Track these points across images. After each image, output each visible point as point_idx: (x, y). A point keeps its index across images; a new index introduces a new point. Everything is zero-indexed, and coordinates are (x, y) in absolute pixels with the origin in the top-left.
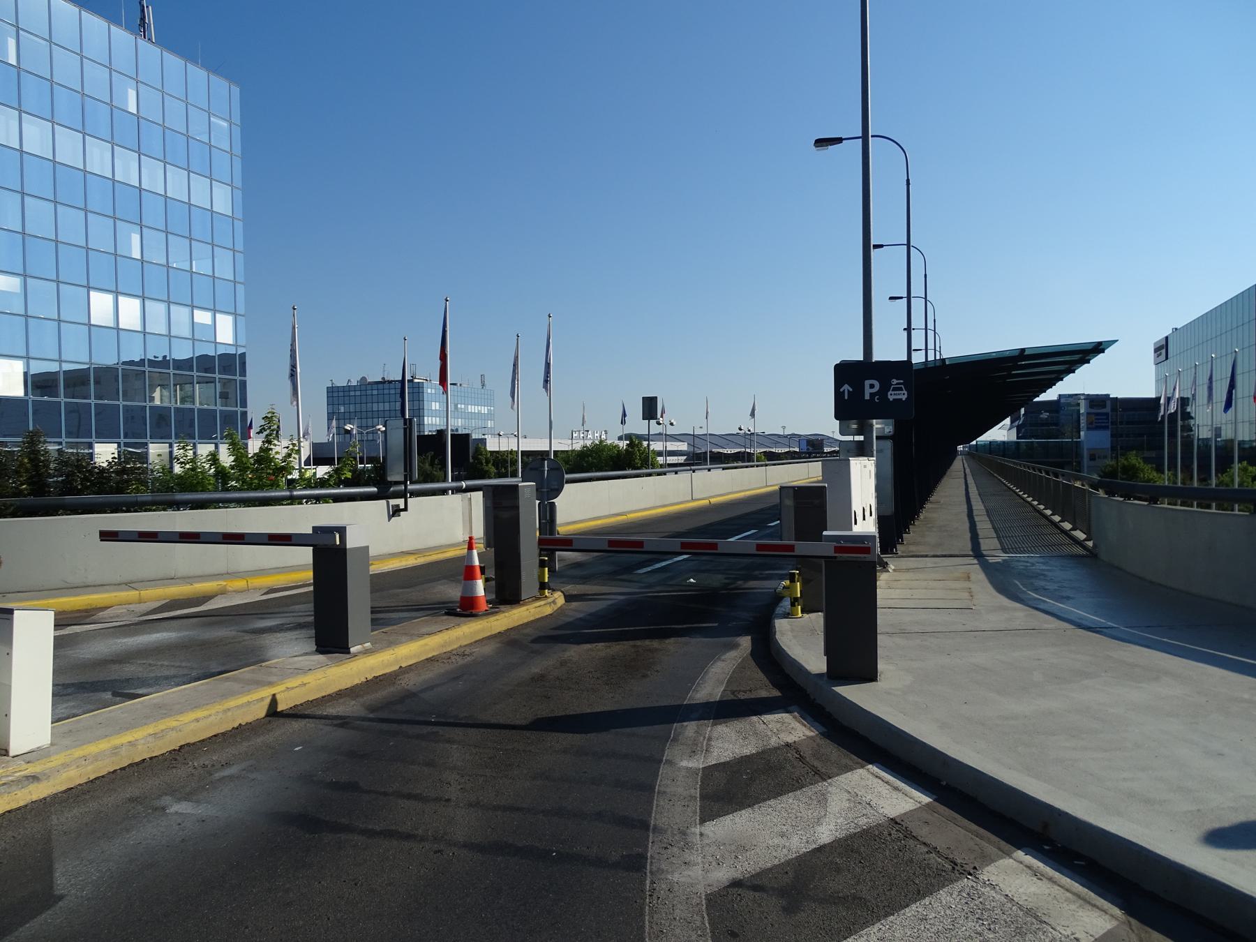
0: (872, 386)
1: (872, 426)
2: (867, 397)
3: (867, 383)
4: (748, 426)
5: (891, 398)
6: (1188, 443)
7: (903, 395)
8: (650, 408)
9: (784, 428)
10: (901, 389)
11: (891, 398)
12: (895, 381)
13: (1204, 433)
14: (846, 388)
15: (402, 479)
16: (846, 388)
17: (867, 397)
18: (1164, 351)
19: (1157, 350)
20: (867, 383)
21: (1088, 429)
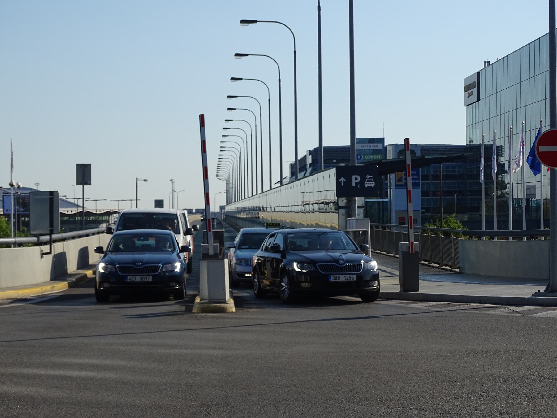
0: (356, 179)
1: (355, 200)
2: (354, 185)
3: (354, 177)
4: (35, 187)
5: (366, 185)
6: (503, 206)
7: (373, 184)
8: (84, 174)
9: (37, 184)
10: (371, 181)
11: (366, 185)
12: (368, 177)
13: (519, 192)
14: (342, 179)
15: (48, 232)
16: (342, 179)
17: (354, 185)
18: (475, 90)
19: (468, 88)
20: (354, 177)
21: (397, 186)
